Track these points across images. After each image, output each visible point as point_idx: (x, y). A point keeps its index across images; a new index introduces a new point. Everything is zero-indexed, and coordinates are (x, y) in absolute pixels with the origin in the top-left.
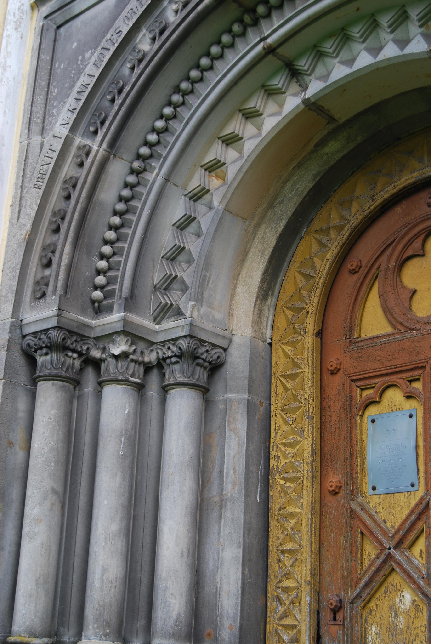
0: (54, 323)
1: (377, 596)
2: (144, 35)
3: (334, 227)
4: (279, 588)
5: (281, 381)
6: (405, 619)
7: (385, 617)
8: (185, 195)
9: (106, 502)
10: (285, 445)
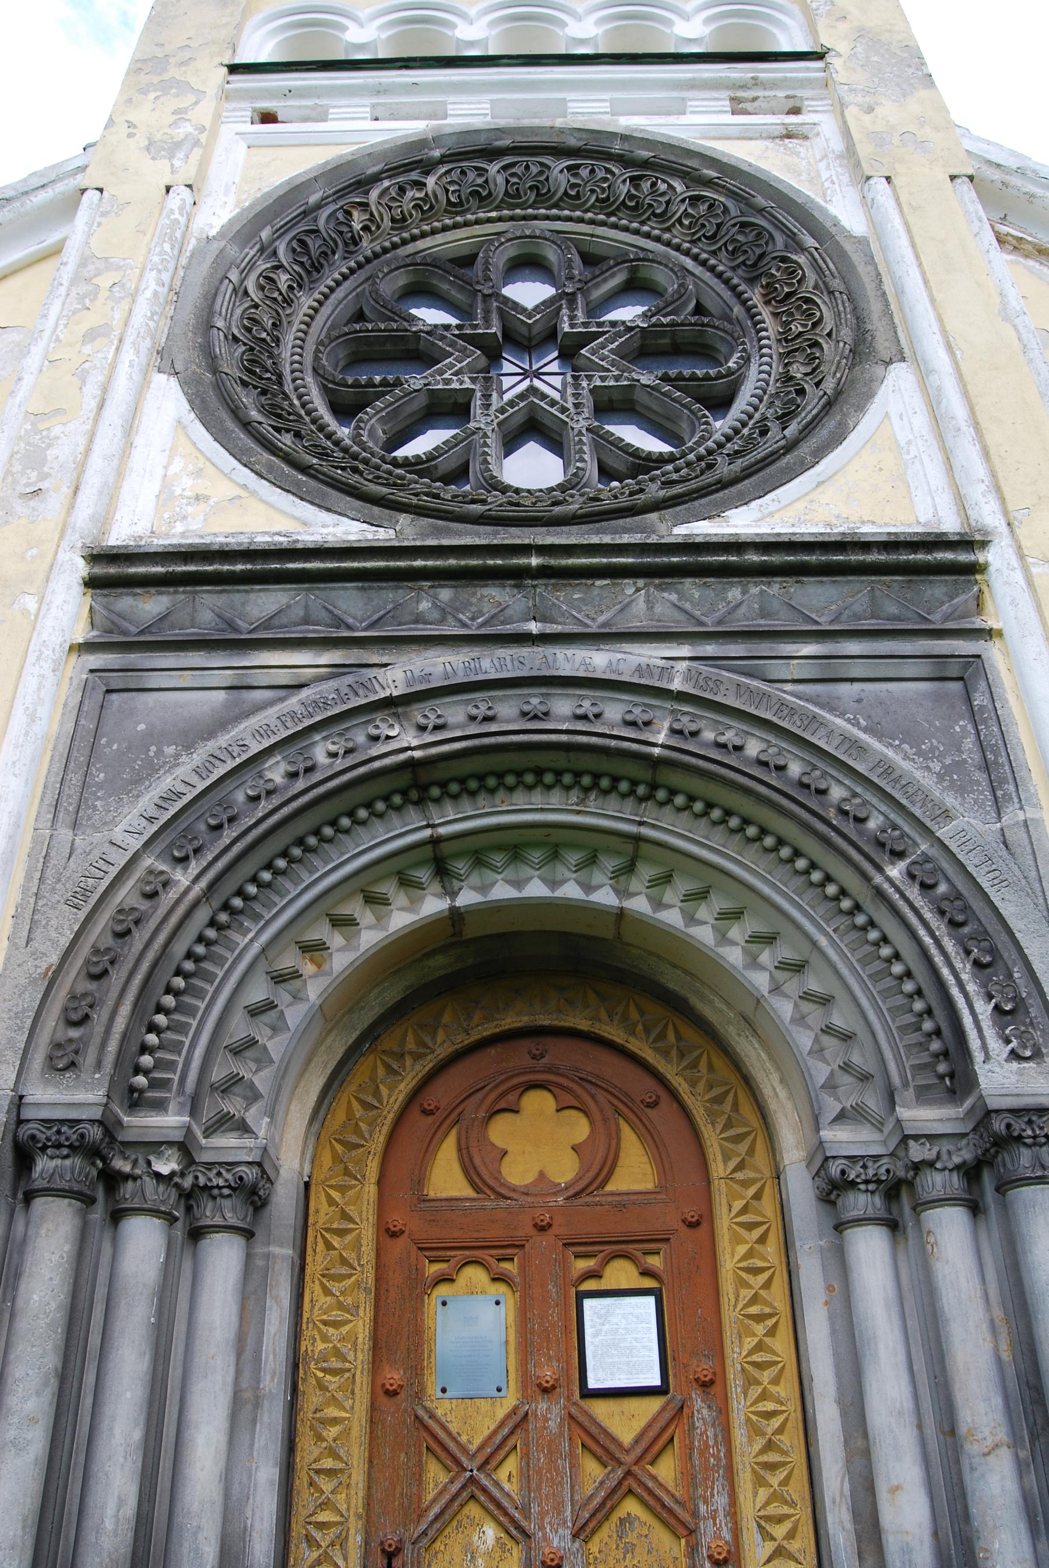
0: (97, 1114)
1: (446, 1533)
2: (278, 762)
3: (411, 1053)
4: (310, 1523)
5: (323, 1236)
6: (486, 1562)
7: (457, 1560)
8: (267, 973)
9: (129, 1395)
10: (325, 1323)
